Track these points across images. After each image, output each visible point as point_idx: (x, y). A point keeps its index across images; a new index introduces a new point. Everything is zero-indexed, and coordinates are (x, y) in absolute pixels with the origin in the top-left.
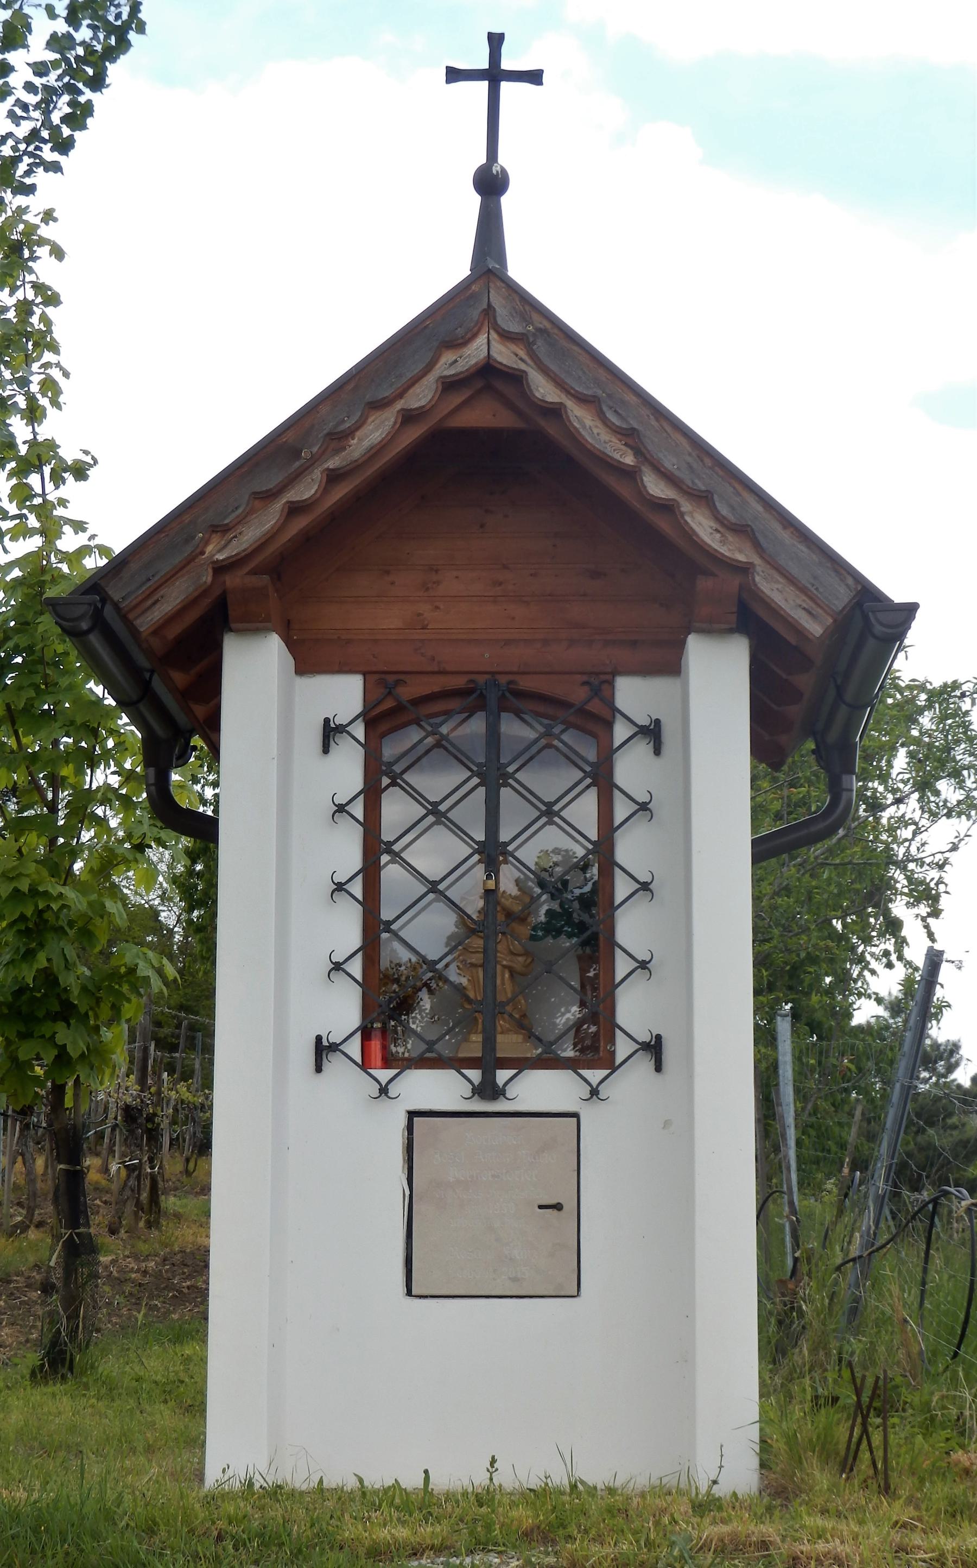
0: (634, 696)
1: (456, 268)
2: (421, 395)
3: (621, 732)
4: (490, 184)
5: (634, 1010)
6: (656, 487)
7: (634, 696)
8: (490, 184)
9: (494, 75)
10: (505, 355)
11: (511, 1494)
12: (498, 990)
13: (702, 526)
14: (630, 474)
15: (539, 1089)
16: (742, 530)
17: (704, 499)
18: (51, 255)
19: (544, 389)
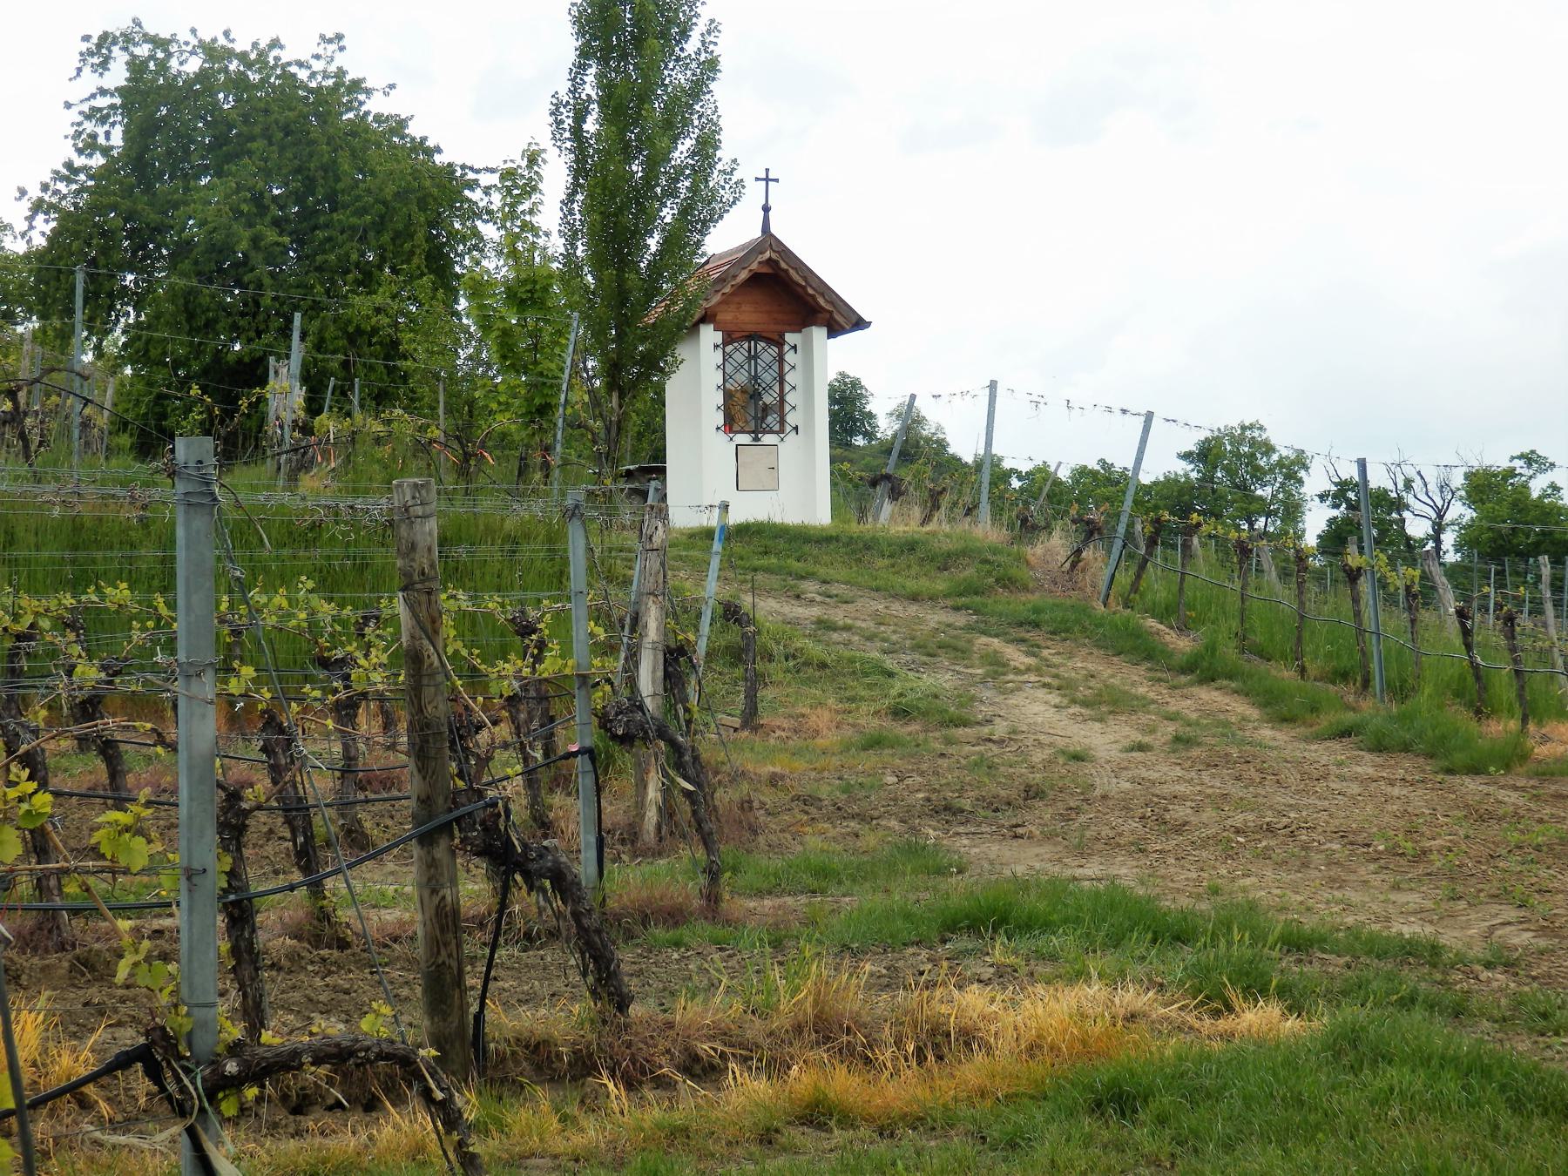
0: (790, 338)
1: (757, 233)
2: (754, 266)
3: (786, 348)
4: (766, 209)
5: (791, 419)
6: (810, 291)
7: (790, 338)
8: (766, 209)
9: (767, 180)
10: (774, 256)
11: (1540, 762)
12: (752, 411)
13: (821, 301)
14: (804, 288)
15: (768, 439)
16: (832, 303)
17: (822, 295)
18: (1103, 462)
19: (783, 265)
